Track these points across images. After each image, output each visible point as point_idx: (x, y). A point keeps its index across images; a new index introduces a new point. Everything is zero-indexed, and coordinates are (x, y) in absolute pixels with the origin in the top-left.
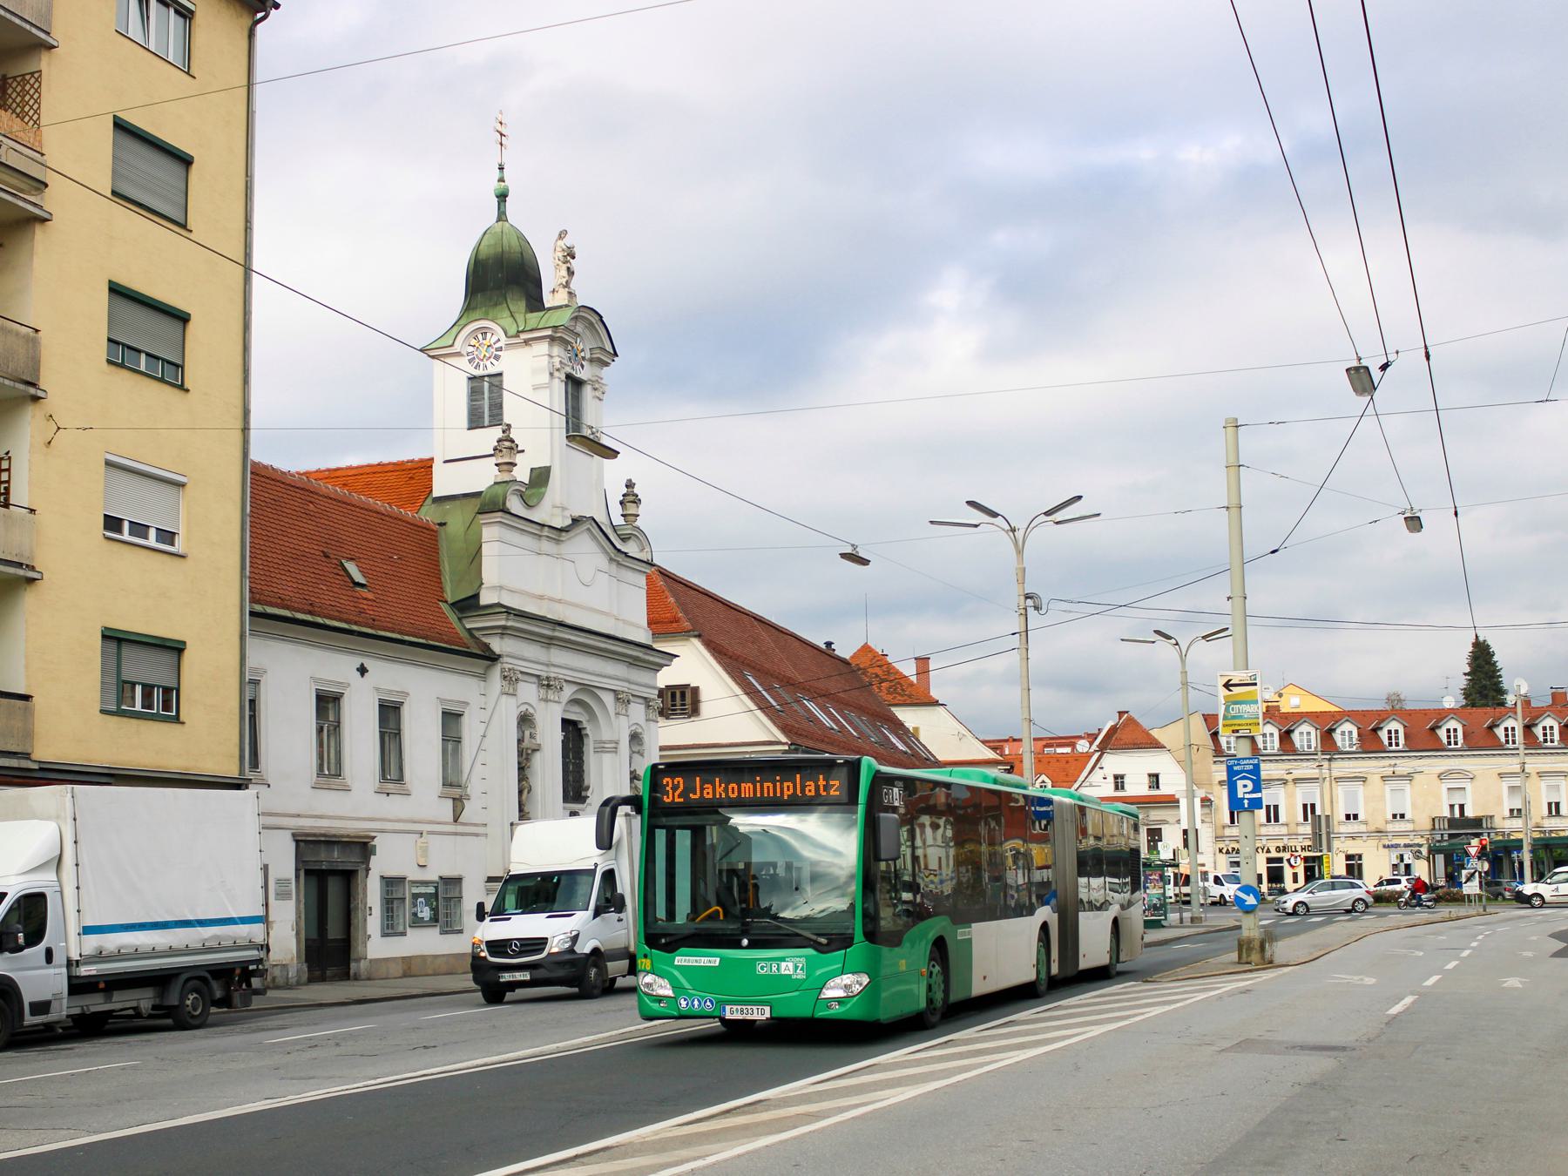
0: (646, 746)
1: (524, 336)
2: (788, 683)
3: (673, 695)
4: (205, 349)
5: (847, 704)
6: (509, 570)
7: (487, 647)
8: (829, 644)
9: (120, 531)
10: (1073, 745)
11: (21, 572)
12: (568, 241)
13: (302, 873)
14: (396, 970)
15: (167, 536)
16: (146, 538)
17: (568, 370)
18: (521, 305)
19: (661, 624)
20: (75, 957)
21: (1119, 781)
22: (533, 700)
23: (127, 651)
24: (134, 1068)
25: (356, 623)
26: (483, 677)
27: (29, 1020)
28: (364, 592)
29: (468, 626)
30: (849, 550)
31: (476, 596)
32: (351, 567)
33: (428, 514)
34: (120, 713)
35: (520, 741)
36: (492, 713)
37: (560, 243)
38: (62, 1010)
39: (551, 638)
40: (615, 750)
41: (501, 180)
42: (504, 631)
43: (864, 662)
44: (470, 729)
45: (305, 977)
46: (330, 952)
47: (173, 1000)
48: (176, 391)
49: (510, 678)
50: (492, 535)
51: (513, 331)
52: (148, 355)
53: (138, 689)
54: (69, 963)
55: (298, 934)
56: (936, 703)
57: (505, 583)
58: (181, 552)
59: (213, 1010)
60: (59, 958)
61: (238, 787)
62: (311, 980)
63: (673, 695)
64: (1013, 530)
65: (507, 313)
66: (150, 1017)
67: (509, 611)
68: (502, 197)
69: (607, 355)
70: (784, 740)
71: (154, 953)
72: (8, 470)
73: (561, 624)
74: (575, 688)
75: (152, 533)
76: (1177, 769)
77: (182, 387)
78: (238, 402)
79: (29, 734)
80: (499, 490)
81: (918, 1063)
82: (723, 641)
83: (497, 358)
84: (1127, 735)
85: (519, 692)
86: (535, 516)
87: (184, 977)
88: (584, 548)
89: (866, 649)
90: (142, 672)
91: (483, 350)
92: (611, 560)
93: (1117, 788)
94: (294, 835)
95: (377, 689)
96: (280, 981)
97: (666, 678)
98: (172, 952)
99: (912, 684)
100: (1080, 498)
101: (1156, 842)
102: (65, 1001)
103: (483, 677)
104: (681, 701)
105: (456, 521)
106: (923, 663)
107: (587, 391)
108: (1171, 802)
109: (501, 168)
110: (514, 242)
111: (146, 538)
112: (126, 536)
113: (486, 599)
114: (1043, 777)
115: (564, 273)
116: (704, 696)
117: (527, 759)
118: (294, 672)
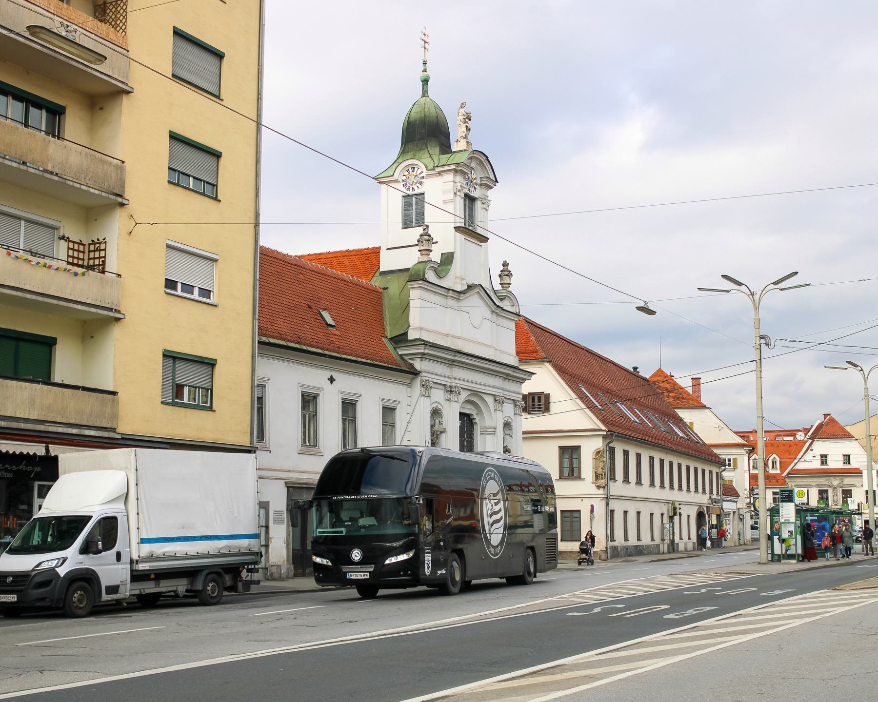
0: (514, 431)
1: (438, 169)
2: (608, 392)
3: (533, 399)
4: (231, 175)
5: (646, 407)
6: (427, 317)
7: (412, 366)
8: (635, 368)
9: (175, 289)
10: (794, 436)
11: (111, 314)
12: (467, 109)
15: (206, 293)
16: (192, 293)
17: (466, 191)
18: (436, 150)
19: (526, 353)
20: (135, 557)
21: (824, 459)
22: (442, 401)
23: (179, 365)
24: (160, 631)
25: (327, 350)
27: (105, 597)
28: (333, 330)
30: (642, 305)
31: (406, 334)
32: (326, 315)
33: (376, 282)
34: (173, 404)
35: (432, 426)
37: (462, 111)
38: (127, 591)
39: (453, 361)
40: (494, 433)
41: (425, 71)
42: (422, 356)
43: (658, 379)
44: (400, 418)
45: (292, 573)
47: (199, 587)
48: (212, 201)
49: (427, 387)
50: (416, 295)
51: (431, 166)
52: (194, 178)
53: (186, 389)
54: (132, 562)
55: (288, 546)
56: (704, 407)
57: (423, 326)
58: (214, 303)
59: (225, 593)
60: (125, 558)
61: (249, 452)
62: (296, 575)
63: (533, 399)
64: (752, 294)
65: (427, 155)
66: (185, 597)
67: (426, 343)
68: (425, 81)
69: (491, 182)
70: (603, 428)
71: (187, 557)
72: (105, 250)
73: (460, 352)
74: (469, 393)
75: (196, 291)
76: (862, 451)
77: (216, 199)
78: (252, 209)
79: (115, 416)
80: (421, 266)
81: (672, 641)
82: (565, 365)
83: (421, 183)
84: (830, 429)
85: (432, 396)
86: (444, 283)
87: (206, 572)
88: (475, 305)
89: (660, 372)
90: (187, 376)
91: (412, 178)
92: (493, 312)
93: (822, 463)
94: (286, 483)
95: (341, 392)
96: (276, 575)
97: (528, 388)
98: (198, 556)
99: (689, 395)
100: (797, 273)
101: (847, 498)
102: (128, 586)
103: (409, 385)
104: (538, 403)
105: (394, 286)
106: (696, 382)
107: (478, 205)
108: (858, 473)
109: (425, 63)
110: (433, 111)
111: (192, 293)
112: (179, 292)
113: (412, 335)
114: (774, 456)
115: (464, 129)
116: (552, 399)
117: (437, 438)
118: (287, 380)
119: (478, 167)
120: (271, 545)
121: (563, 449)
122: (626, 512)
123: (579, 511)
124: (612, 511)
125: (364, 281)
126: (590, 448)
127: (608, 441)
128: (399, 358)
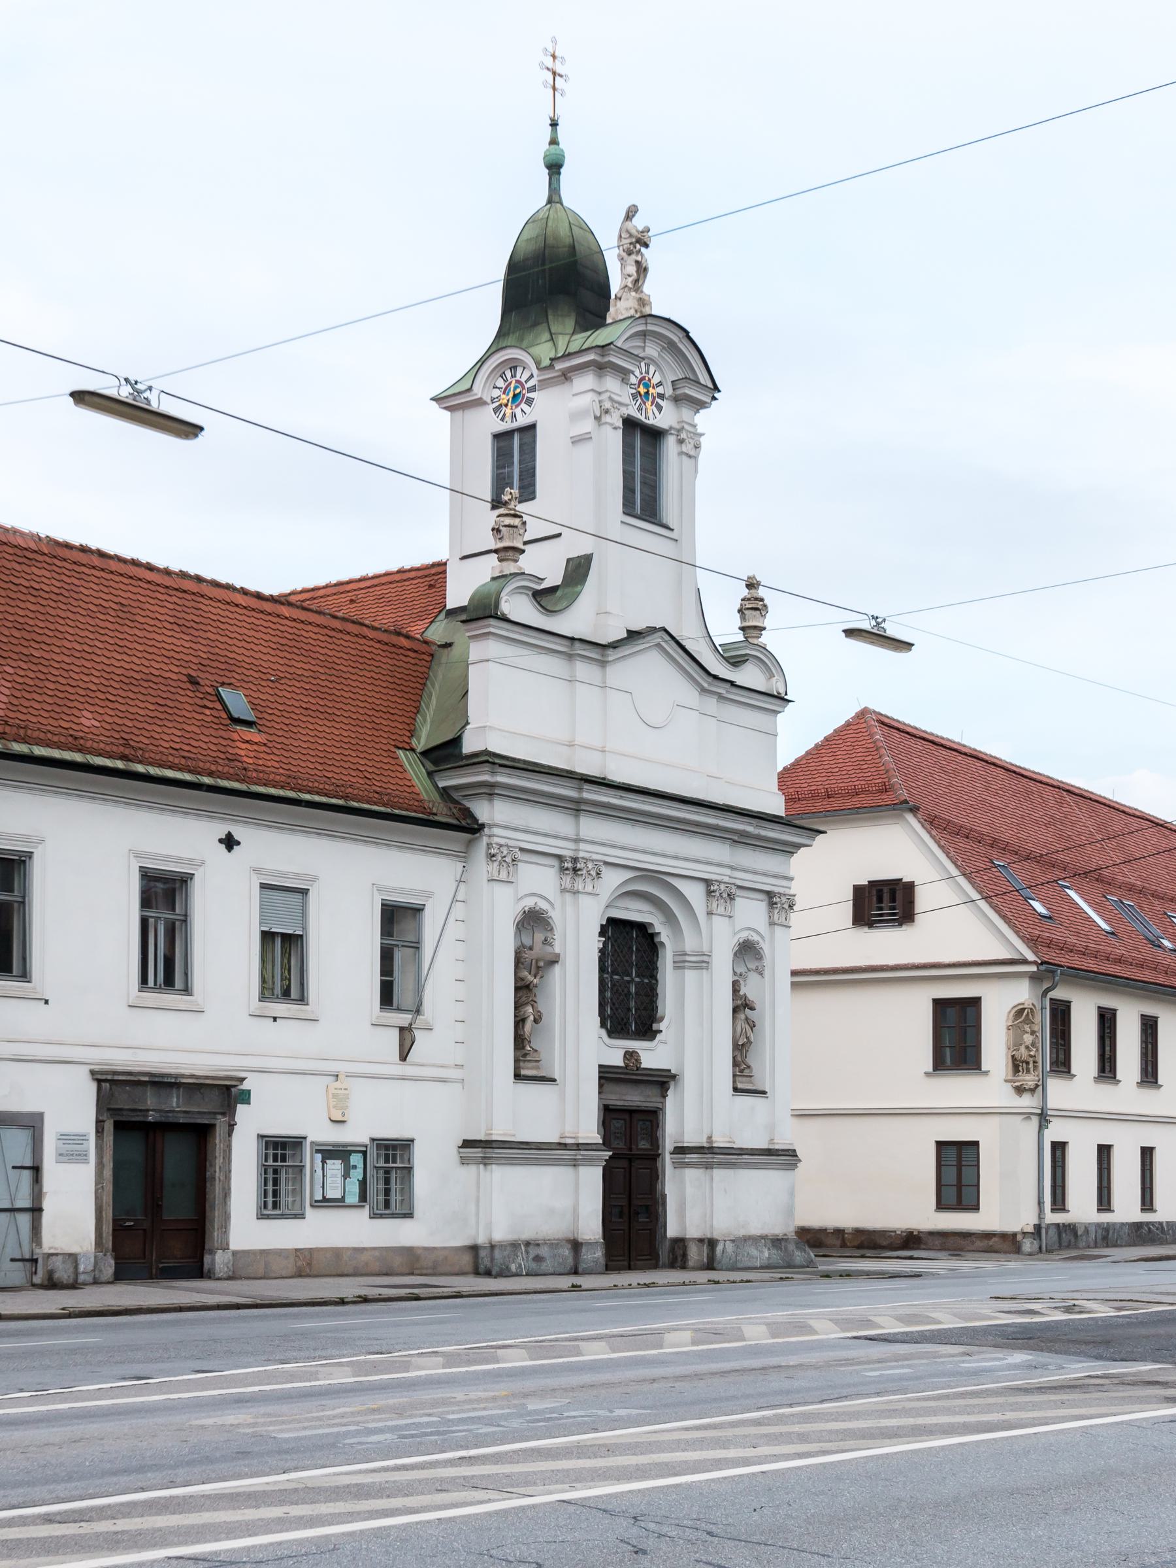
0: (767, 962)
1: (559, 366)
6: (510, 703)
7: (468, 813)
12: (638, 223)
13: (109, 1126)
14: (290, 1266)
17: (633, 411)
26: (464, 855)
28: (251, 734)
29: (441, 784)
31: (456, 741)
33: (437, 632)
36: (472, 913)
39: (578, 802)
41: (554, 142)
46: (635, 1232)
49: (506, 860)
62: (121, 1275)
65: (546, 336)
70: (1031, 957)
74: (630, 875)
80: (496, 584)
83: (529, 402)
94: (92, 1072)
95: (138, 856)
104: (884, 902)
107: (670, 446)
109: (554, 124)
110: (563, 231)
119: (668, 357)
120: (46, 1204)
121: (941, 1006)
122: (1104, 1151)
123: (976, 1144)
124: (1059, 1148)
125: (416, 630)
126: (999, 1005)
127: (1046, 986)
128: (435, 796)
